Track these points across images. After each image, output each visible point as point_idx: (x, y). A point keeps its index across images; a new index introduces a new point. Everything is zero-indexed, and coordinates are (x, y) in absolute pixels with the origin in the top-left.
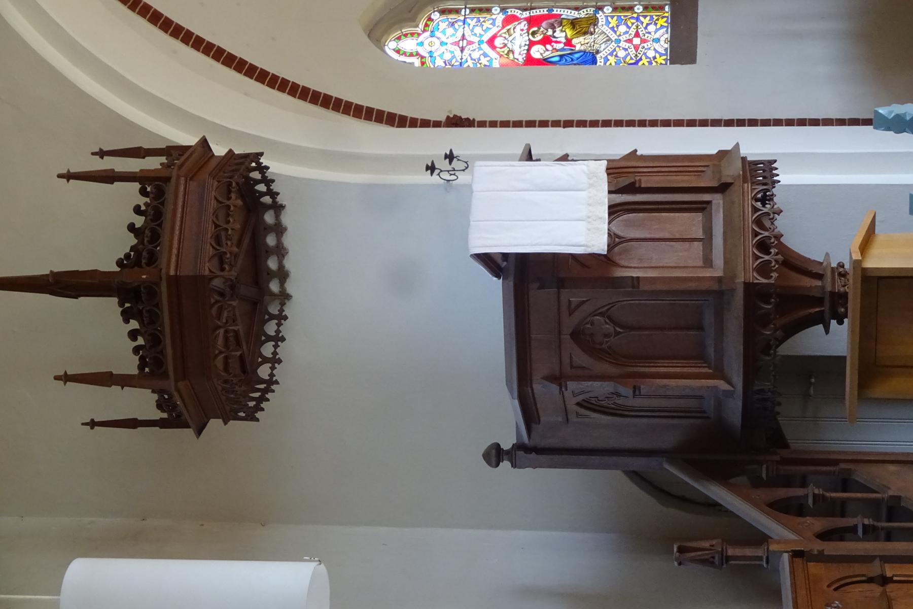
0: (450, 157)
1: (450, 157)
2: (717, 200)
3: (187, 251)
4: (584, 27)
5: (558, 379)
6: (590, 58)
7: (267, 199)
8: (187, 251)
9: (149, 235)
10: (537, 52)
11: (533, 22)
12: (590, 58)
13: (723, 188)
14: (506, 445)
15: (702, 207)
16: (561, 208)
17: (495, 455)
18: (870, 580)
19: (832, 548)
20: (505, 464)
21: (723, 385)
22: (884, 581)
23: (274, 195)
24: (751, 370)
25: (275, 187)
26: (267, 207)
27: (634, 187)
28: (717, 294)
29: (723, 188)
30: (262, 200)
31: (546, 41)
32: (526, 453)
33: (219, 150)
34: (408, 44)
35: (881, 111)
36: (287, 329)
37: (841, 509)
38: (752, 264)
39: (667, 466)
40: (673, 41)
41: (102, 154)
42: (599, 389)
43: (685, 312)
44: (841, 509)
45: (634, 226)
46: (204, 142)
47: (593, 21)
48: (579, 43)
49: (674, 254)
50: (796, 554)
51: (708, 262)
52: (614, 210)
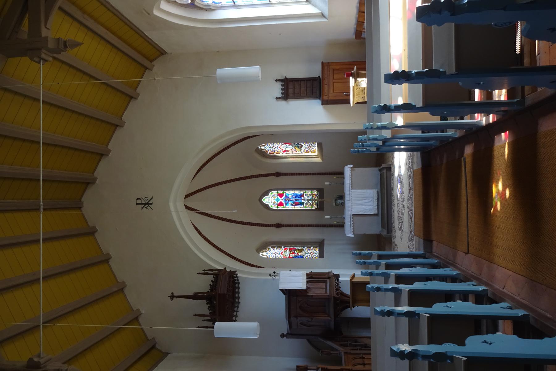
0: (274, 272)
1: (274, 272)
2: (328, 280)
3: (222, 289)
4: (301, 251)
5: (296, 317)
6: (302, 257)
7: (237, 281)
8: (222, 289)
9: (214, 286)
10: (291, 256)
11: (290, 249)
12: (302, 257)
13: (329, 278)
14: (285, 334)
15: (325, 282)
16: (297, 280)
17: (283, 336)
18: (360, 358)
19: (352, 352)
20: (285, 338)
21: (329, 318)
22: (363, 358)
23: (238, 280)
24: (336, 315)
25: (239, 278)
26: (236, 283)
27: (311, 278)
28: (328, 299)
29: (329, 278)
30: (351, 78)
31: (293, 253)
32: (289, 335)
33: (228, 270)
34: (264, 254)
35: (393, 348)
36: (239, 309)
37: (356, 346)
38: (335, 293)
39: (309, 9)
40: (319, 254)
41: (205, 270)
42: (304, 319)
43: (323, 301)
44: (356, 346)
45: (312, 285)
46: (225, 268)
47: (303, 250)
48: (300, 254)
49: (319, 291)
50: (345, 353)
51: (326, 292)
52: (308, 282)
